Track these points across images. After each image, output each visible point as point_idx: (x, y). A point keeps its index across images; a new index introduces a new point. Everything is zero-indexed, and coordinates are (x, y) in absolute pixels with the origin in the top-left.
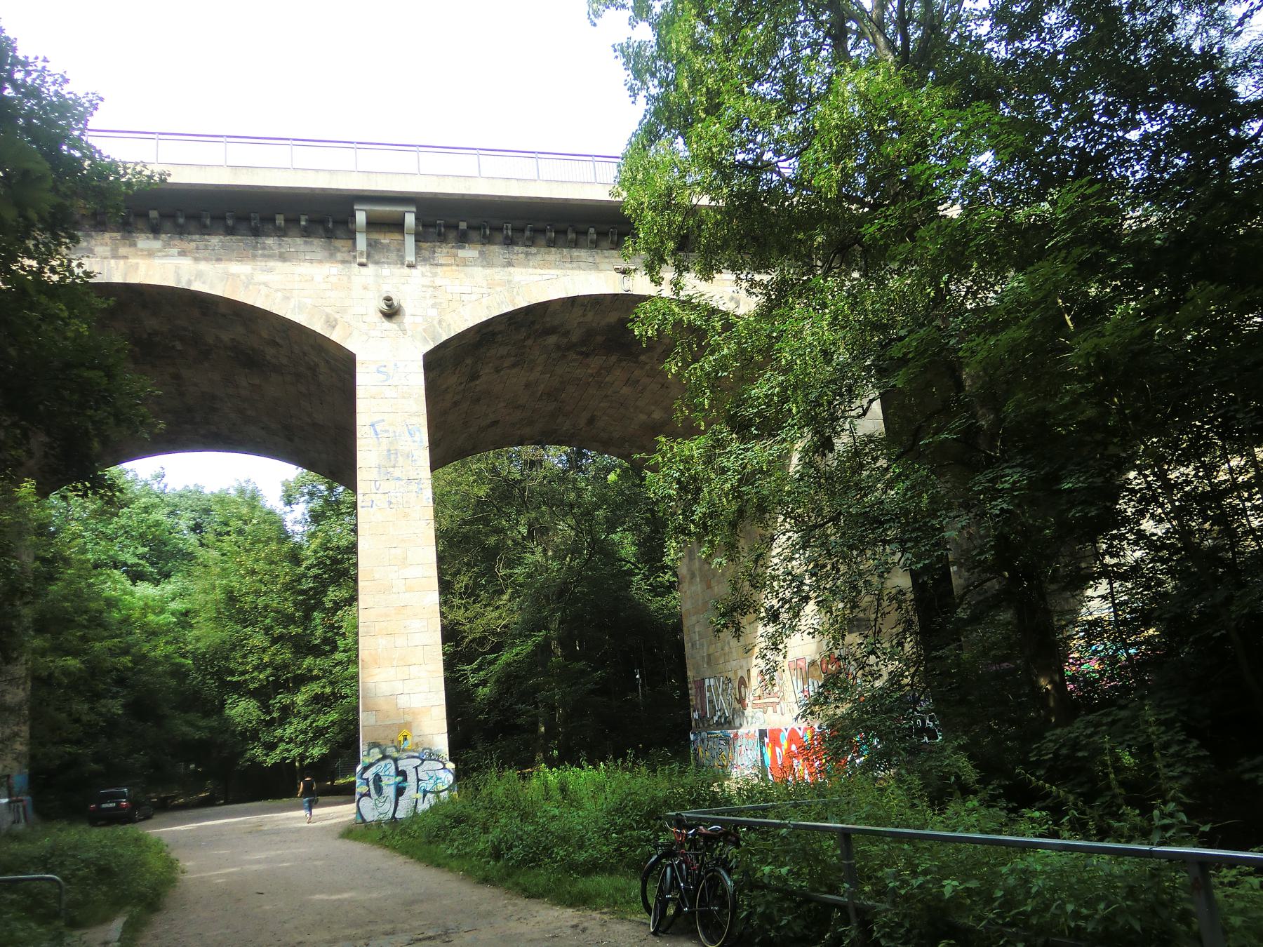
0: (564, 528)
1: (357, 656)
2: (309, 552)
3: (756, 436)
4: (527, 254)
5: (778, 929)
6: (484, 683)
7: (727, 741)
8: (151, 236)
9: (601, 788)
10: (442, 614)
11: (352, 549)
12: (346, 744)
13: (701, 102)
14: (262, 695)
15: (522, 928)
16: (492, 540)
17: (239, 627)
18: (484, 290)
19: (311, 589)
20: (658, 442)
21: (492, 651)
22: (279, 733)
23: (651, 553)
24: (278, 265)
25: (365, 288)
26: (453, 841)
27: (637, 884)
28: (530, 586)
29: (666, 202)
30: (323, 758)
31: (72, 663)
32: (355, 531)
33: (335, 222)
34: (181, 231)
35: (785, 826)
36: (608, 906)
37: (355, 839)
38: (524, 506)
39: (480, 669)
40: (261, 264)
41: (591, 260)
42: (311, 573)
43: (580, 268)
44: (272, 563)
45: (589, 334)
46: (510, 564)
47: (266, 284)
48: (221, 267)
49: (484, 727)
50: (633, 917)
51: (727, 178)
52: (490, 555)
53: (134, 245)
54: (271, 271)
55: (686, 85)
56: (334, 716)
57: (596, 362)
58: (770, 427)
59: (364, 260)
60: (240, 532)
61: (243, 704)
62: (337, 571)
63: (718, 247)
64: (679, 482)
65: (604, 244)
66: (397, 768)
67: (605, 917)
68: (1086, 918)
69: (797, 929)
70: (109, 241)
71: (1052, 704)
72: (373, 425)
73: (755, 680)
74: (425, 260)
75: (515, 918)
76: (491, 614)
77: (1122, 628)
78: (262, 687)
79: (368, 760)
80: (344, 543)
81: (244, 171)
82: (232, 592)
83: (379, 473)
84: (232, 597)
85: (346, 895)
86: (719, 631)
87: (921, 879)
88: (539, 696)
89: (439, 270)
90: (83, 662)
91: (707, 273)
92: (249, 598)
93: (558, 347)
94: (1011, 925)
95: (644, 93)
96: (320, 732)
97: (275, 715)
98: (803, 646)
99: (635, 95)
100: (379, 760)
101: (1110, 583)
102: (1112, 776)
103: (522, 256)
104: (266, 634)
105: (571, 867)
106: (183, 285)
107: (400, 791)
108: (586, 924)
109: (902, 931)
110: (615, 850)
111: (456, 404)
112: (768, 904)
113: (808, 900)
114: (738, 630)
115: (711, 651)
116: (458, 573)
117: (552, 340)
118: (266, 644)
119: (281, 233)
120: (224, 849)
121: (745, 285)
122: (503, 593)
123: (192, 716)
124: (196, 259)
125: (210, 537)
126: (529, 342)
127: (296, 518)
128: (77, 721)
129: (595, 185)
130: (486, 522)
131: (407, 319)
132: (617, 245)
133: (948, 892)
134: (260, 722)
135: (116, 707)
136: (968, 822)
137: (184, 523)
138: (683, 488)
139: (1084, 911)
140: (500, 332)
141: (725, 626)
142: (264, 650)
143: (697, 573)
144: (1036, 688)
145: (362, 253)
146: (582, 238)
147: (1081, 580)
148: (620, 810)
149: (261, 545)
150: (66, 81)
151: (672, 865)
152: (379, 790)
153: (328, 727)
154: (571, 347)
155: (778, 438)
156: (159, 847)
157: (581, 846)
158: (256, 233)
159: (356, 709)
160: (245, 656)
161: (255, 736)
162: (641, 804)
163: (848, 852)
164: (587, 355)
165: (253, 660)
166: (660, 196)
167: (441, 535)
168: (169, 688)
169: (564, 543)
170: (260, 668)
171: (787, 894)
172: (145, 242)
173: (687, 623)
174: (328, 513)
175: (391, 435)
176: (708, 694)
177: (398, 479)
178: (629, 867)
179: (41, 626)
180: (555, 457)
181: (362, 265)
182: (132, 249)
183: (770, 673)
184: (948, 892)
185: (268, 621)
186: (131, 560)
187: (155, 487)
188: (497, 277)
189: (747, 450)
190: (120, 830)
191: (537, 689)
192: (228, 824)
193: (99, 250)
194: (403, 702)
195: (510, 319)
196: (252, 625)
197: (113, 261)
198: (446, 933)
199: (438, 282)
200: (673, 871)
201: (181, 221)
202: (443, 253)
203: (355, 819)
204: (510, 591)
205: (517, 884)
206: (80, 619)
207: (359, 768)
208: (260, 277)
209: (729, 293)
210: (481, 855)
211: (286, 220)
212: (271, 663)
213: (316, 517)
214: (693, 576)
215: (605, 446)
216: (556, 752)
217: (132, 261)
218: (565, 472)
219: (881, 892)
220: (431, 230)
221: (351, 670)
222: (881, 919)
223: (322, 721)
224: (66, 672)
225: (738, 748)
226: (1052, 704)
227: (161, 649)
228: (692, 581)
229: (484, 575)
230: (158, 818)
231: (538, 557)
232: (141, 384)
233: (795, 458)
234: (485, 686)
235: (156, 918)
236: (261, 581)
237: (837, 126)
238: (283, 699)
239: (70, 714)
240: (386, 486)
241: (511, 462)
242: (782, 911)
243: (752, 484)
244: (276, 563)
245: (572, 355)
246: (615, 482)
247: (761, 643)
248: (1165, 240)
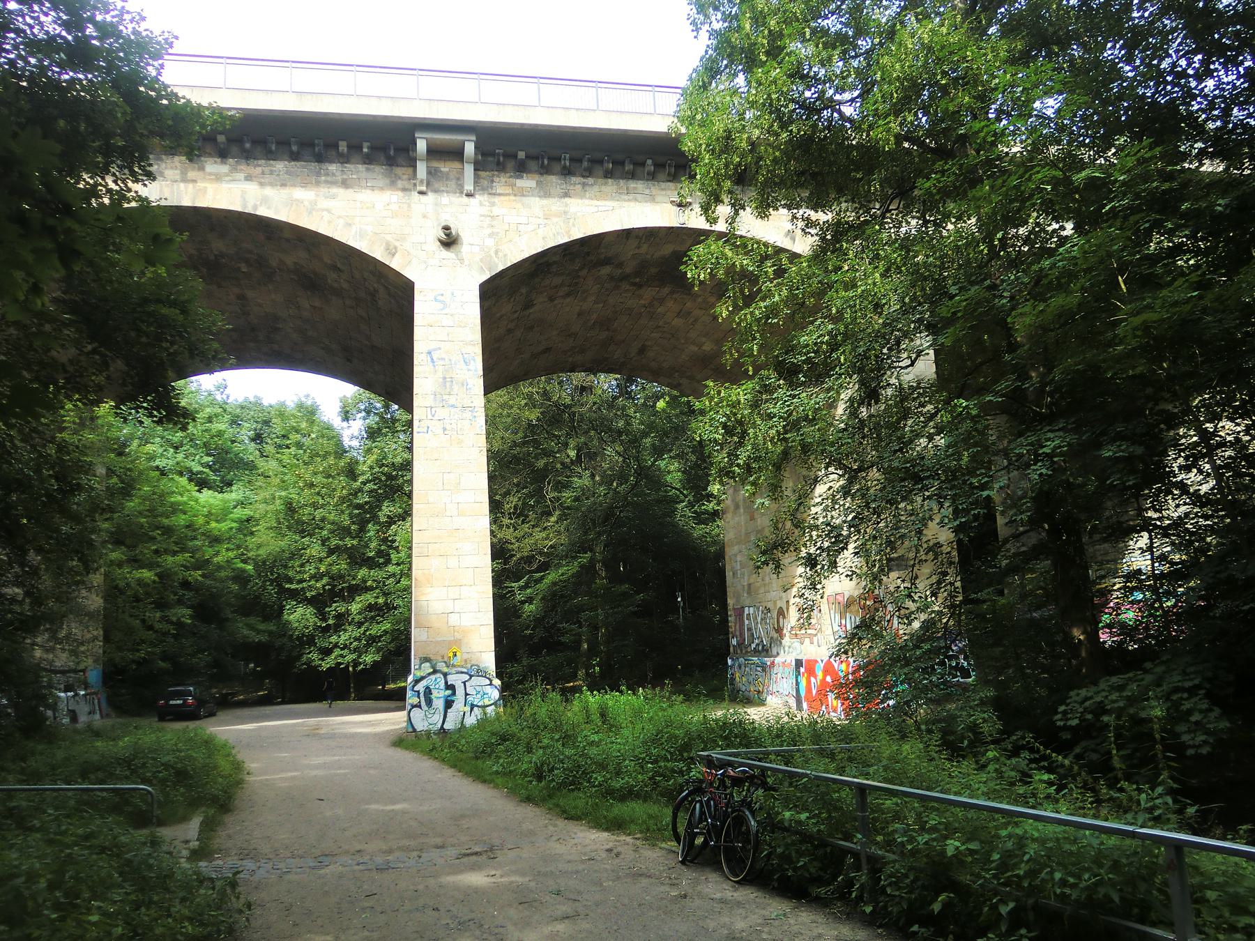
0: (612, 453)
1: (410, 569)
2: (366, 466)
3: (803, 384)
4: (584, 185)
5: (795, 869)
6: (530, 600)
7: (764, 668)
8: (219, 160)
9: (638, 713)
10: (492, 532)
11: (407, 466)
12: (398, 653)
13: (763, 45)
14: (319, 603)
15: (559, 849)
16: (541, 463)
17: (298, 538)
18: (541, 221)
19: (366, 503)
20: (707, 386)
21: (537, 571)
22: (334, 639)
23: (696, 482)
24: (340, 192)
25: (424, 217)
26: (498, 757)
27: (668, 812)
28: (577, 509)
29: (726, 143)
30: (375, 663)
31: (147, 574)
32: (410, 449)
33: (396, 150)
34: (247, 156)
35: (806, 775)
36: (641, 832)
37: (407, 749)
38: (573, 431)
39: (526, 586)
40: (324, 190)
41: (647, 192)
42: (366, 488)
43: (636, 200)
44: (329, 476)
45: (643, 266)
46: (561, 486)
47: (328, 211)
48: (285, 193)
49: (527, 648)
50: (663, 845)
51: (784, 126)
52: (540, 477)
53: (202, 169)
54: (334, 197)
55: (748, 26)
56: (386, 626)
57: (649, 293)
58: (819, 372)
59: (424, 188)
60: (299, 445)
61: (300, 610)
62: (391, 487)
63: (775, 184)
64: (725, 426)
65: (661, 176)
66: (446, 682)
67: (638, 842)
68: (1073, 886)
69: (812, 870)
70: (178, 165)
71: (1083, 654)
72: (429, 353)
73: (793, 616)
74: (483, 189)
75: (554, 838)
76: (539, 535)
77: (1160, 583)
78: (319, 594)
79: (419, 674)
80: (398, 460)
81: (309, 97)
82: (291, 504)
83: (435, 399)
84: (290, 508)
85: (398, 807)
86: (759, 567)
87: (927, 837)
88: (584, 616)
89: (496, 199)
90: (156, 575)
91: (763, 210)
92: (308, 510)
93: (611, 278)
94: (1005, 885)
95: (706, 27)
96: (373, 640)
97: (331, 622)
98: (840, 585)
99: (697, 30)
100: (429, 674)
101: (1150, 538)
102: (1114, 752)
103: (579, 186)
104: (323, 545)
105: (610, 793)
106: (249, 210)
107: (449, 704)
108: (619, 849)
109: (908, 881)
110: (650, 779)
111: (509, 331)
112: (787, 846)
113: (824, 844)
114: (778, 567)
115: (752, 581)
116: (508, 493)
117: (606, 271)
118: (324, 554)
119: (344, 159)
120: (288, 752)
121: (801, 224)
122: (550, 514)
123: (252, 620)
124: (262, 184)
125: (270, 449)
126: (584, 273)
127: (352, 433)
128: (150, 628)
129: (654, 116)
130: (536, 443)
131: (465, 248)
132: (674, 178)
133: (950, 852)
134: (316, 628)
135: (184, 614)
136: (970, 788)
137: (246, 432)
138: (729, 431)
139: (1071, 880)
140: (555, 262)
141: (766, 563)
142: (321, 560)
143: (741, 504)
144: (1069, 638)
145: (422, 181)
146: (639, 170)
147: (1123, 533)
148: (655, 740)
149: (319, 459)
150: (143, 19)
151: (701, 802)
152: (429, 702)
153: (381, 636)
154: (624, 278)
155: (826, 386)
156: (225, 749)
157: (618, 773)
158: (320, 159)
159: (409, 620)
160: (302, 565)
161: (311, 641)
162: (676, 737)
163: (863, 805)
164: (640, 286)
165: (310, 569)
166: (718, 139)
167: (492, 456)
168: (230, 592)
169: (611, 469)
170: (317, 577)
171: (806, 837)
172: (213, 166)
173: (730, 552)
174: (384, 431)
175: (447, 362)
176: (747, 622)
177: (453, 406)
178: (663, 796)
179: (118, 539)
180: (606, 383)
181: (421, 193)
182: (200, 173)
183: (807, 611)
184: (950, 852)
185: (325, 532)
186: (197, 468)
187: (219, 397)
188: (554, 208)
189: (794, 397)
190: (192, 725)
191: (581, 609)
192: (287, 726)
193: (169, 173)
194: (453, 620)
195: (565, 250)
196: (311, 535)
197: (182, 185)
198: (491, 850)
199: (496, 211)
200: (702, 806)
201: (248, 145)
202: (501, 183)
203: (406, 728)
204: (557, 513)
205: (557, 805)
206: (154, 532)
207: (410, 679)
208: (324, 203)
209: (782, 229)
210: (524, 774)
211: (348, 147)
212: (327, 573)
213: (372, 434)
214: (737, 507)
215: (655, 375)
216: (597, 669)
217: (201, 185)
218: (615, 398)
219: (889, 844)
220: (490, 159)
221: (404, 582)
222: (889, 870)
223: (375, 630)
224: (140, 582)
225: (774, 676)
226: (1083, 654)
227: (223, 555)
228: (737, 518)
229: (532, 497)
230: (222, 715)
231: (586, 481)
232: (213, 317)
233: (840, 409)
234: (531, 603)
235: (228, 819)
236: (318, 494)
237: (898, 78)
238: (338, 607)
239: (143, 621)
240: (442, 413)
241: (563, 388)
242: (801, 854)
243: (798, 430)
244: (333, 478)
245: (625, 286)
246: (663, 410)
247: (801, 582)
248: (1226, 206)
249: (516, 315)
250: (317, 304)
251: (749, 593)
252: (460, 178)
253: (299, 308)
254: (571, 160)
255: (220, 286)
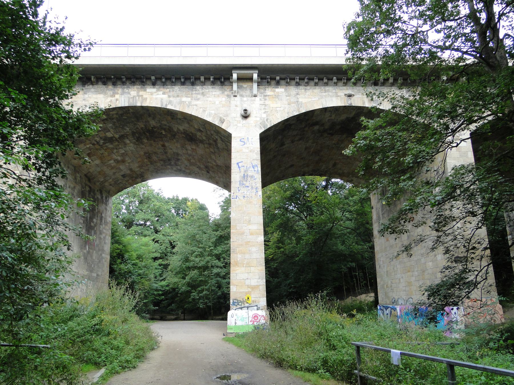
4: (305, 89)
8: (152, 87)
33: (224, 79)
41: (334, 91)
70: (136, 89)
72: (238, 164)
106: (164, 106)
117: (316, 128)
126: (307, 129)
129: (338, 55)
146: (330, 82)
158: (193, 84)
164: (332, 135)
182: (145, 92)
188: (292, 100)
208: (194, 102)
220: (264, 81)
249: (277, 149)
250: (194, 147)
251: (387, 275)
252: (251, 88)
253: (187, 150)
254: (300, 79)
255: (154, 141)
